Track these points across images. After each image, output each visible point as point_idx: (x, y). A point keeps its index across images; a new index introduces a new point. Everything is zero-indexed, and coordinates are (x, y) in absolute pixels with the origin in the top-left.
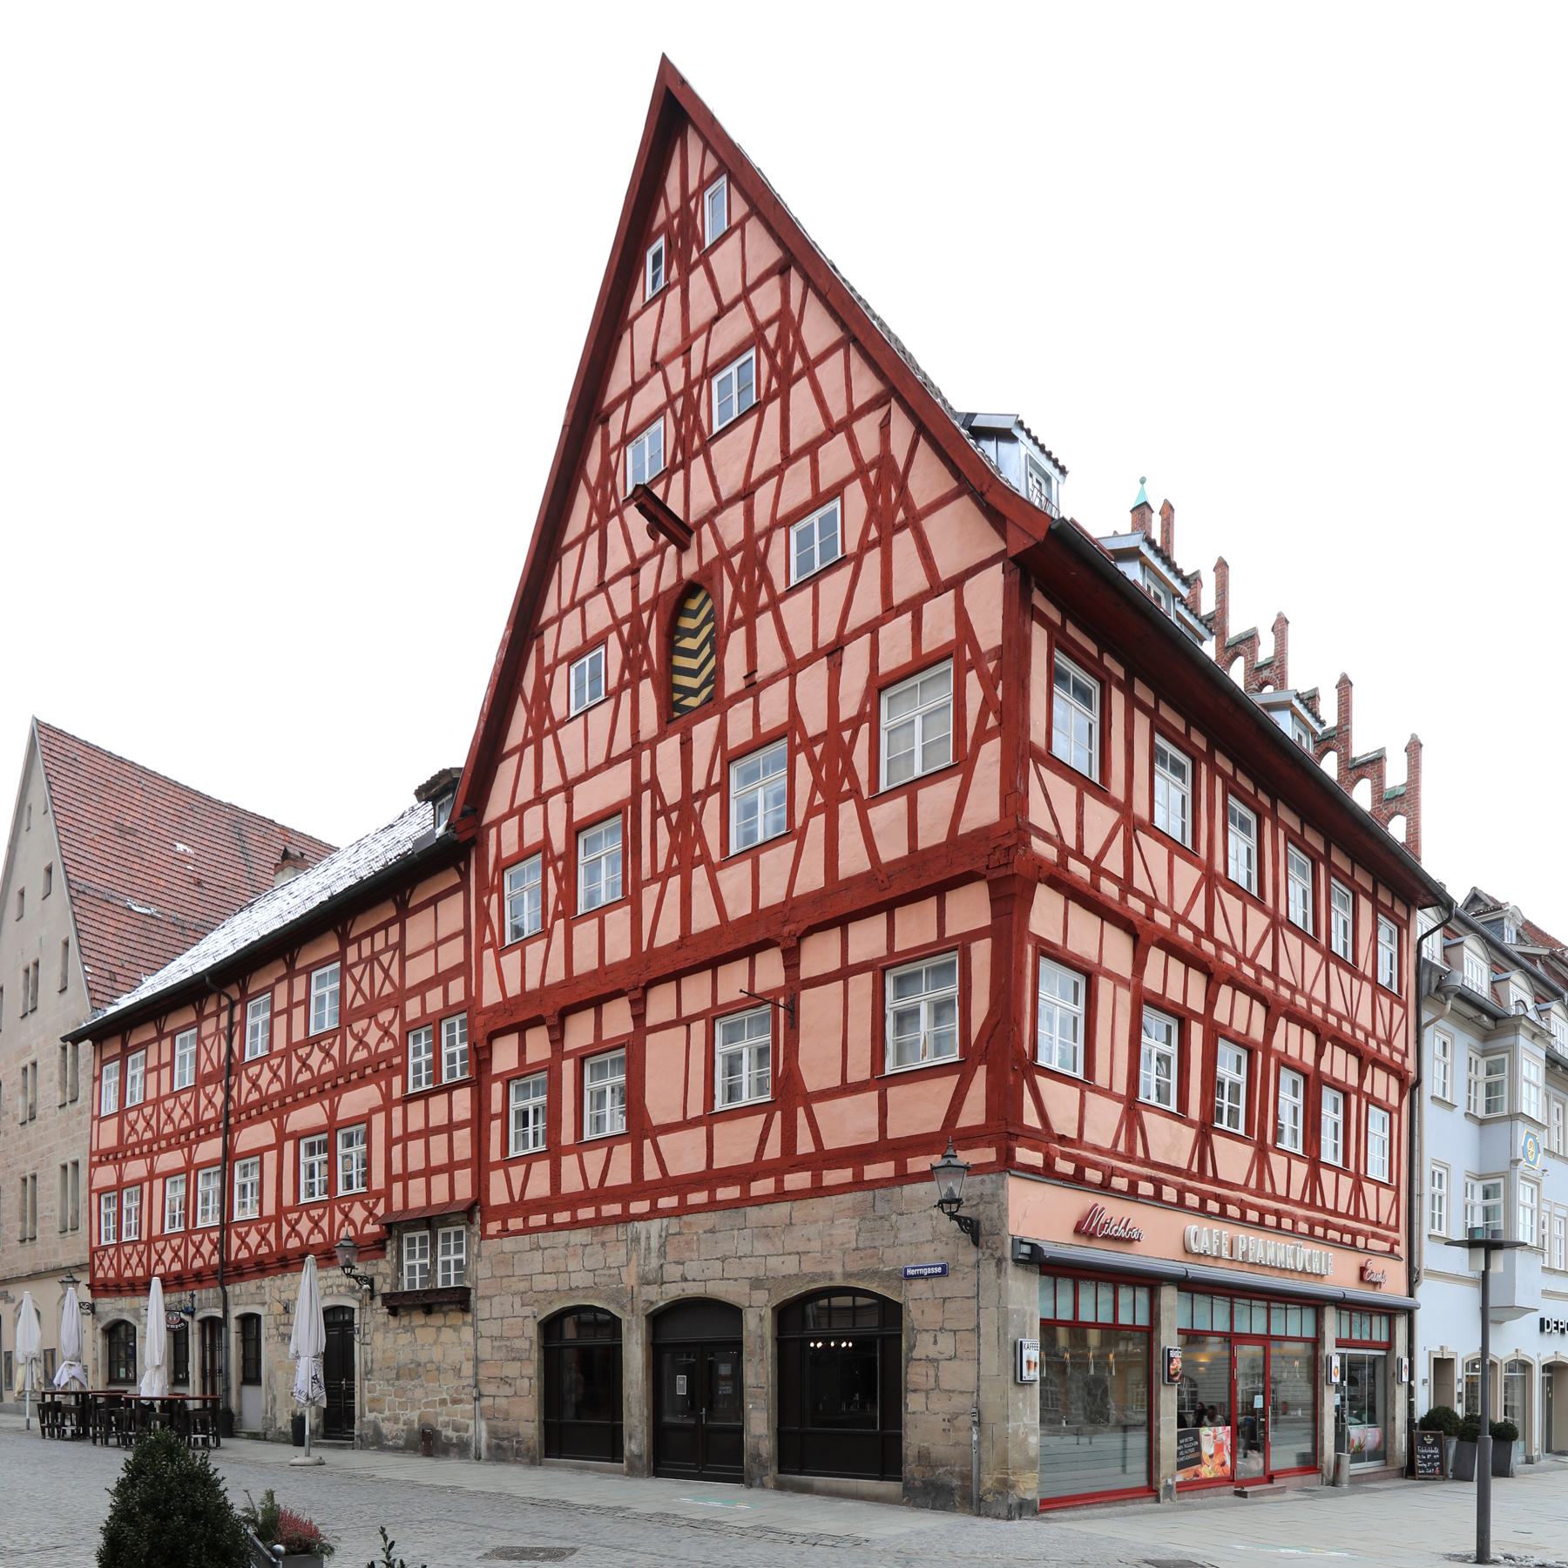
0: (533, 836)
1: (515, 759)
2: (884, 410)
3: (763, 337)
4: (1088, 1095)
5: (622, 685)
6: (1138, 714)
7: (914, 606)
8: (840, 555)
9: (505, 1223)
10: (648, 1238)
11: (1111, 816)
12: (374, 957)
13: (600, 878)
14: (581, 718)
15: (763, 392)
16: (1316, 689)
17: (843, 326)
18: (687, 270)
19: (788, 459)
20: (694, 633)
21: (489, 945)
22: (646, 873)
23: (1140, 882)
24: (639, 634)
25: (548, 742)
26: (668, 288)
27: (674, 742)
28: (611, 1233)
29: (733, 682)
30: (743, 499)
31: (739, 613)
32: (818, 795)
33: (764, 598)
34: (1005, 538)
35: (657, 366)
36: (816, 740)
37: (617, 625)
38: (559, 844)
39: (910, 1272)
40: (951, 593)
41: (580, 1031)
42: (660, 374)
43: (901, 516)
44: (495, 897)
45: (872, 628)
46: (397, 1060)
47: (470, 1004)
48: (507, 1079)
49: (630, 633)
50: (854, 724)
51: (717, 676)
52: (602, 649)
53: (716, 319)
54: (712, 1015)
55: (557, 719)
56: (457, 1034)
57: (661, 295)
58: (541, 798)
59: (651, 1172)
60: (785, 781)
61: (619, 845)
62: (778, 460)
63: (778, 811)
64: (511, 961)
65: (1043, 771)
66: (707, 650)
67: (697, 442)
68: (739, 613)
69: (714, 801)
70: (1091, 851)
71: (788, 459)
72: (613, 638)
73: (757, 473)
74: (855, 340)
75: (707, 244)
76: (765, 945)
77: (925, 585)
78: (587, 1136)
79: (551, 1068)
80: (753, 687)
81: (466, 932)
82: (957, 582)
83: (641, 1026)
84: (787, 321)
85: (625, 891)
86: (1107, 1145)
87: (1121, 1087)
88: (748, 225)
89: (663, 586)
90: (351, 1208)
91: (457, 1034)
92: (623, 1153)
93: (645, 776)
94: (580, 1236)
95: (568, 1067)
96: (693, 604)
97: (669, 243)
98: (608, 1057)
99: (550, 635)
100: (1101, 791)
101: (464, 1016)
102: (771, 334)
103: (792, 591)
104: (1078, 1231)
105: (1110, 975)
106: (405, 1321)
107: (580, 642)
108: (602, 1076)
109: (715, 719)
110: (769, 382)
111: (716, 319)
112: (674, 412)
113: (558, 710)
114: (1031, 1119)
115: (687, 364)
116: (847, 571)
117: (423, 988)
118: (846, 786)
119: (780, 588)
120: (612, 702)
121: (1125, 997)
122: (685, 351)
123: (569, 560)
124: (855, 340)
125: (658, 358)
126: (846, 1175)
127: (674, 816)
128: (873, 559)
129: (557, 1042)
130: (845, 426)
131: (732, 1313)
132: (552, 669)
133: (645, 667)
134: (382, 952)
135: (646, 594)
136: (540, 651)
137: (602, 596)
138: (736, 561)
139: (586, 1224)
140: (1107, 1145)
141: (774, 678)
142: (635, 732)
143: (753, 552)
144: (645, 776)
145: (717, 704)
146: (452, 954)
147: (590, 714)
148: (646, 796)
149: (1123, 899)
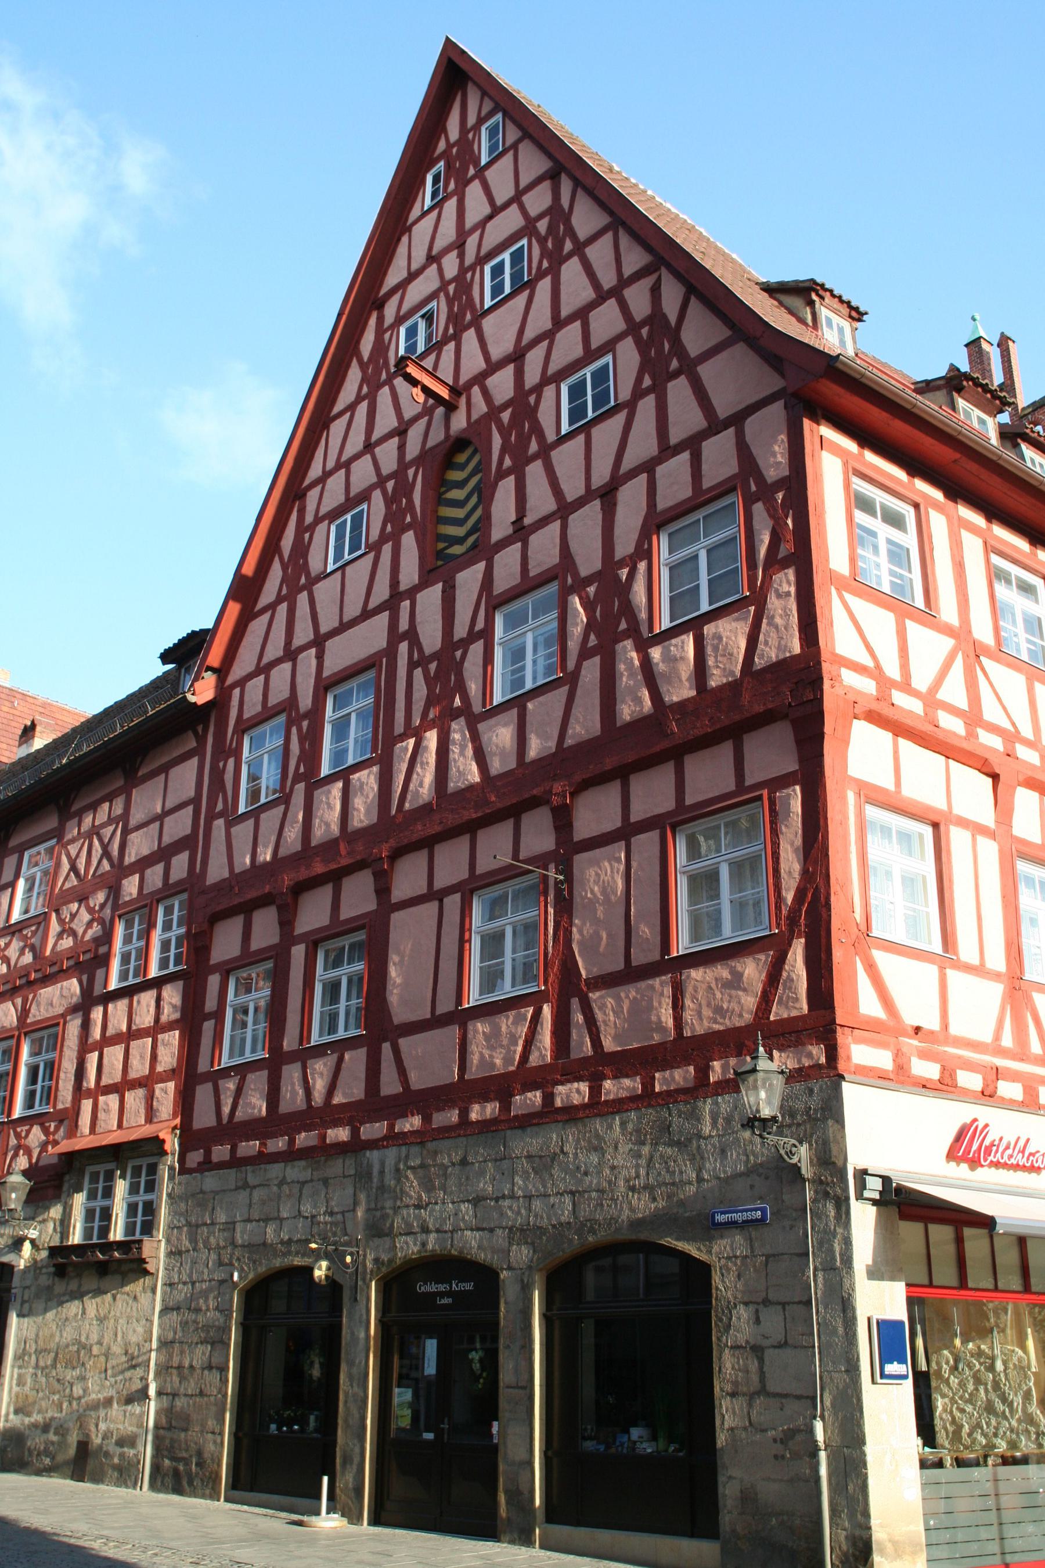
0: (279, 692)
1: (265, 618)
2: (655, 276)
3: (535, 227)
4: (950, 973)
5: (383, 538)
6: (965, 535)
7: (693, 444)
8: (612, 403)
9: (208, 1153)
10: (382, 1172)
11: (948, 643)
12: (95, 831)
13: (345, 733)
14: (339, 574)
15: (534, 272)
16: (952, 365)
17: (611, 213)
18: (464, 183)
19: (559, 323)
20: (461, 485)
21: (221, 815)
22: (399, 728)
23: (991, 712)
24: (404, 488)
25: (303, 598)
26: (445, 199)
27: (436, 590)
28: (337, 1166)
29: (500, 529)
30: (514, 361)
31: (508, 462)
32: (592, 637)
33: (534, 447)
34: (783, 375)
35: (433, 259)
36: (588, 581)
37: (381, 482)
38: (305, 701)
39: (720, 1218)
40: (731, 430)
41: (314, 913)
42: (435, 266)
43: (675, 364)
44: (231, 762)
45: (649, 467)
46: (102, 950)
47: (193, 886)
48: (227, 970)
49: (394, 489)
50: (631, 562)
51: (484, 523)
52: (365, 506)
53: (490, 217)
54: (467, 889)
55: (313, 575)
56: (175, 917)
57: (438, 205)
58: (291, 654)
59: (390, 1085)
60: (555, 624)
61: (370, 700)
62: (549, 325)
63: (549, 656)
64: (243, 832)
65: (847, 596)
66: (474, 500)
67: (468, 317)
68: (508, 462)
69: (477, 649)
70: (921, 681)
71: (559, 323)
72: (377, 496)
73: (529, 334)
74: (623, 224)
75: (483, 162)
76: (533, 803)
77: (704, 424)
78: (315, 1039)
79: (279, 956)
80: (521, 532)
81: (196, 801)
82: (737, 420)
83: (387, 904)
84: (558, 214)
85: (374, 749)
86: (987, 1037)
87: (997, 961)
88: (521, 146)
89: (430, 444)
90: (28, 1132)
91: (175, 917)
92: (356, 1060)
93: (404, 625)
94: (295, 1171)
95: (298, 952)
96: (461, 458)
97: (448, 167)
98: (346, 942)
99: (313, 495)
100: (928, 616)
101: (185, 896)
102: (542, 226)
103: (562, 440)
104: (952, 1155)
105: (963, 823)
106: (73, 1285)
107: (342, 499)
108: (337, 963)
109: (481, 566)
110: (540, 263)
111: (490, 217)
112: (447, 295)
113: (315, 564)
114: (869, 1005)
115: (461, 256)
116: (620, 418)
117: (143, 864)
118: (623, 625)
119: (551, 437)
120: (372, 555)
121: (989, 850)
122: (459, 245)
123: (337, 428)
124: (623, 224)
125: (434, 253)
126: (631, 1085)
127: (433, 667)
128: (647, 405)
129: (286, 923)
130: (616, 292)
131: (485, 1278)
132: (312, 528)
133: (408, 519)
134: (104, 825)
135: (413, 450)
136: (302, 512)
137: (368, 457)
138: (506, 416)
139: (306, 1153)
140: (987, 1037)
141: (543, 522)
142: (394, 582)
143: (524, 403)
144: (404, 625)
145: (484, 550)
146: (179, 825)
147: (348, 569)
148: (404, 647)
149: (971, 735)
